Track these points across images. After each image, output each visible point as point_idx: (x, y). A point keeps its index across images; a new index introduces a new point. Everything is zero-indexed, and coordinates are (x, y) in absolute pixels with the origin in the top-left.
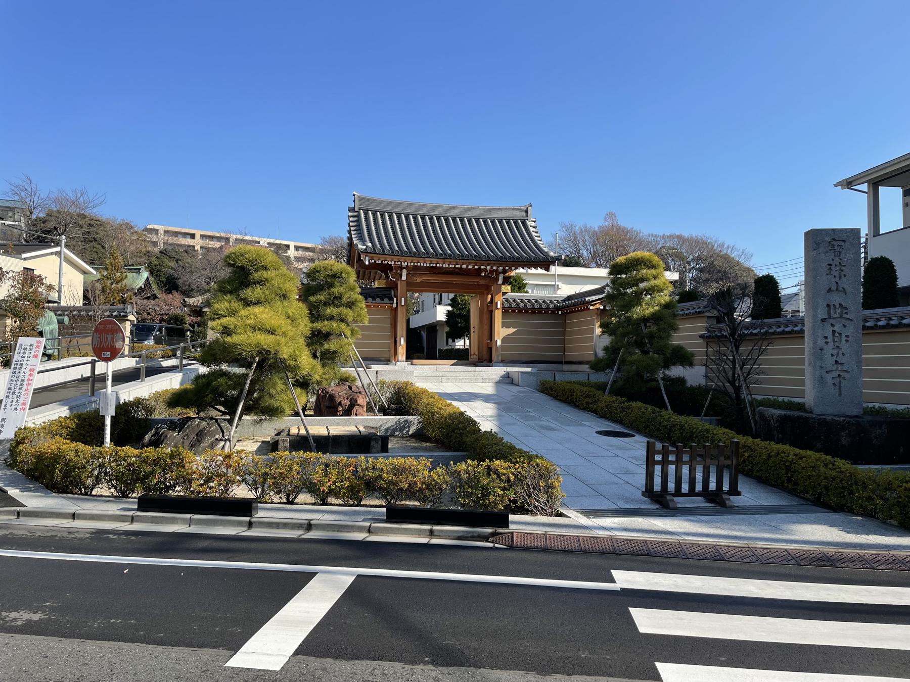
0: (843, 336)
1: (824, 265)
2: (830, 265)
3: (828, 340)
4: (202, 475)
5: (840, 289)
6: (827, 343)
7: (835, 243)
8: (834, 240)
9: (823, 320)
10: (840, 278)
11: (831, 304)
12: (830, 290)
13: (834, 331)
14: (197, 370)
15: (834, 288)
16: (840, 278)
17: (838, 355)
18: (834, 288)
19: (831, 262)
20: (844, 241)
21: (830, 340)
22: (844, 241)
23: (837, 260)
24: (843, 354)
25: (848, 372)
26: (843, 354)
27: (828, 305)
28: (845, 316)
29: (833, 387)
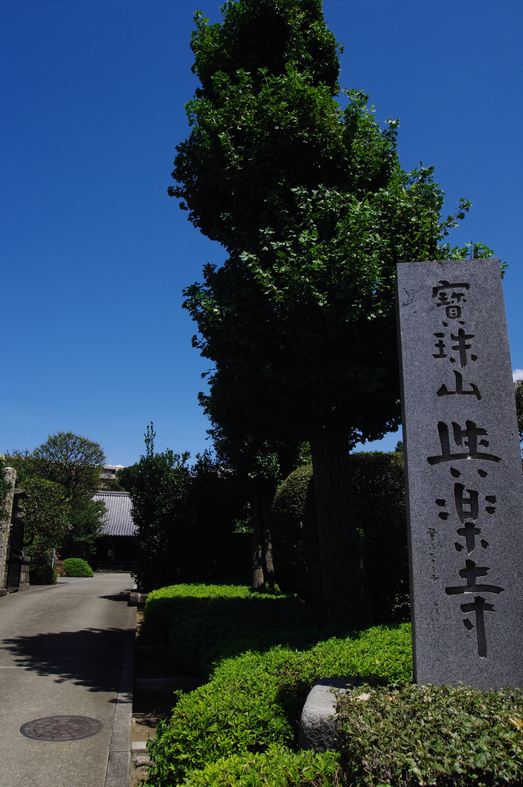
0: (481, 498)
1: (429, 336)
2: (440, 335)
3: (487, 504)
4: (416, 301)
5: (467, 387)
6: (444, 516)
7: (447, 291)
8: (446, 284)
9: (432, 460)
10: (464, 363)
11: (448, 423)
12: (443, 391)
13: (459, 488)
14: (419, 781)
15: (452, 386)
16: (464, 363)
17: (471, 546)
18: (452, 386)
19: (442, 329)
20: (467, 286)
21: (450, 508)
22: (467, 286)
23: (454, 326)
24: (484, 544)
25: (498, 590)
26: (484, 544)
27: (442, 427)
28: (481, 449)
29: (464, 629)
